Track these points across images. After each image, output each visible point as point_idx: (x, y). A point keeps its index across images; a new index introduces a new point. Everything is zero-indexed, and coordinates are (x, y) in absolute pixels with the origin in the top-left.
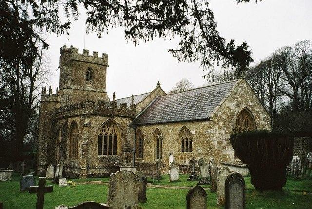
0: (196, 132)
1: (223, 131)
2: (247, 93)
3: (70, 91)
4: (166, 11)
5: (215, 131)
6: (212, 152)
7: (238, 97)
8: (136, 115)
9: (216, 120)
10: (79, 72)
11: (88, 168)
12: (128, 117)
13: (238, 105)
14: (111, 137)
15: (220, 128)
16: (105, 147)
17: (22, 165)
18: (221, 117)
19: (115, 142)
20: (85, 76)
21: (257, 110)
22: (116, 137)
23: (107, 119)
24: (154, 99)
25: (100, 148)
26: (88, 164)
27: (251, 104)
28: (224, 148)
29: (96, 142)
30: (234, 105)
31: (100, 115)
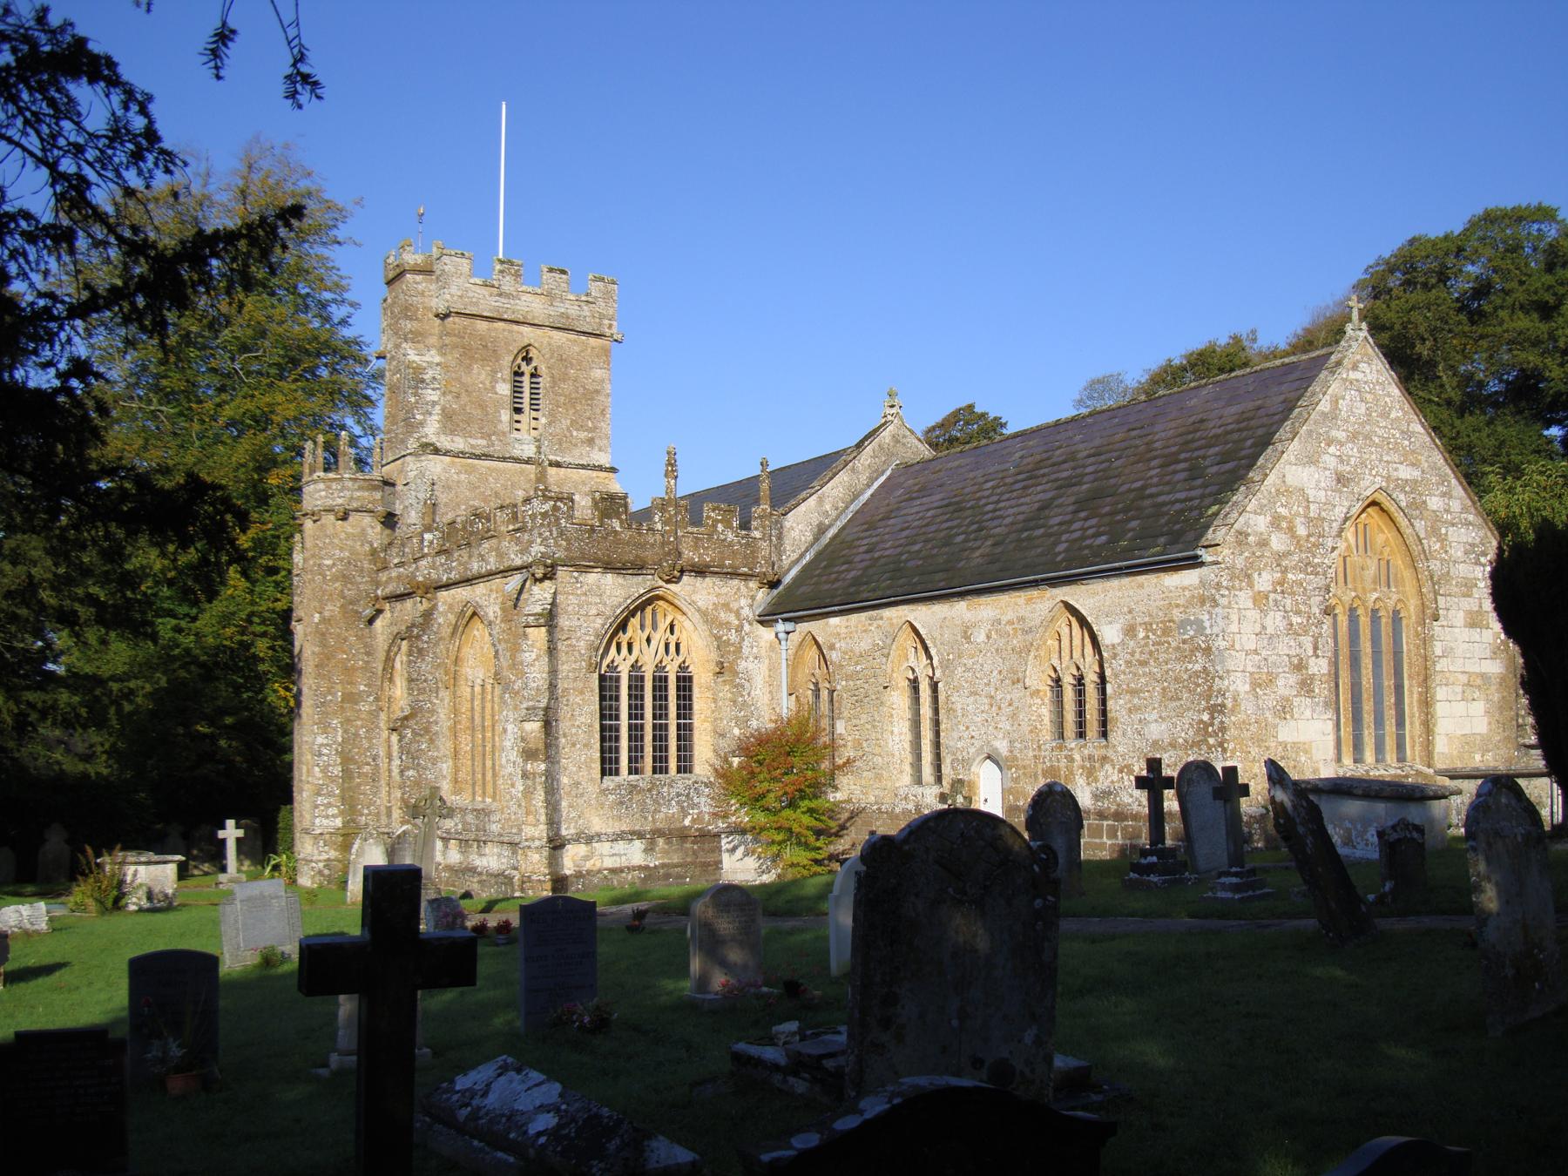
0: (1130, 631)
1: (1275, 621)
2: (1385, 415)
3: (435, 466)
4: (23, 612)
5: (1234, 617)
6: (1223, 729)
7: (1341, 435)
8: (786, 562)
9: (1240, 562)
10: (480, 374)
11: (556, 845)
12: (746, 577)
13: (1341, 479)
14: (660, 683)
15: (1260, 600)
16: (636, 733)
17: (221, 834)
18: (1264, 544)
19: (685, 709)
20: (504, 389)
21: (1435, 503)
22: (685, 683)
23: (637, 586)
24: (872, 480)
25: (608, 735)
26: (553, 822)
27: (1405, 473)
28: (1284, 710)
29: (581, 716)
30: (1327, 479)
31: (609, 567)
